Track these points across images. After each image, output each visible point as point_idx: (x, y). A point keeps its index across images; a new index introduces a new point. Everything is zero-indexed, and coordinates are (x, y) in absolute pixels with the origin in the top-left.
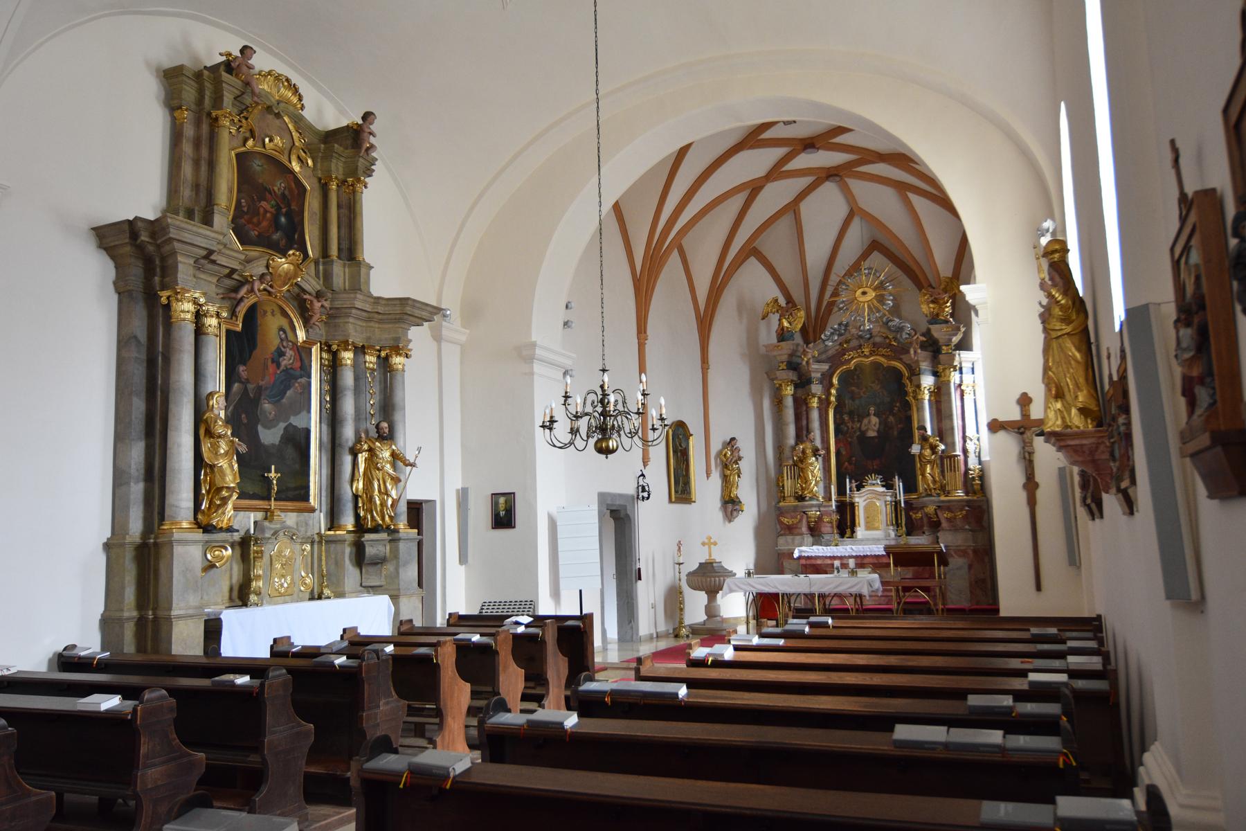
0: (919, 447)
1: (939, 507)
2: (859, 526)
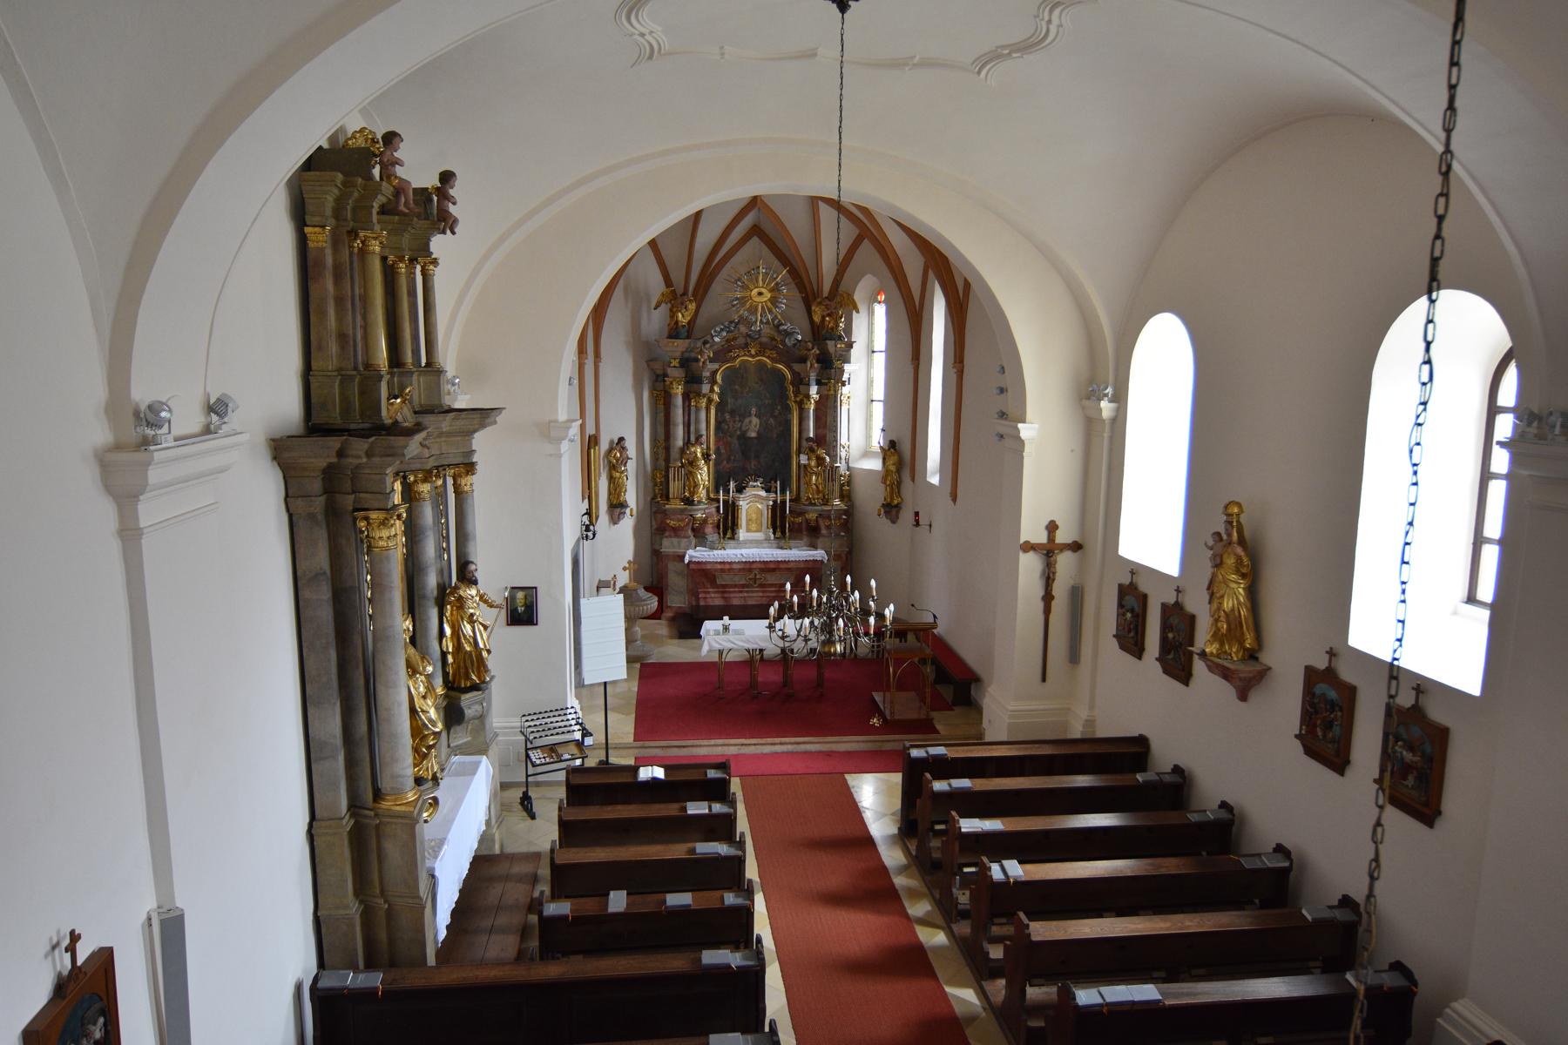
1: (820, 515)
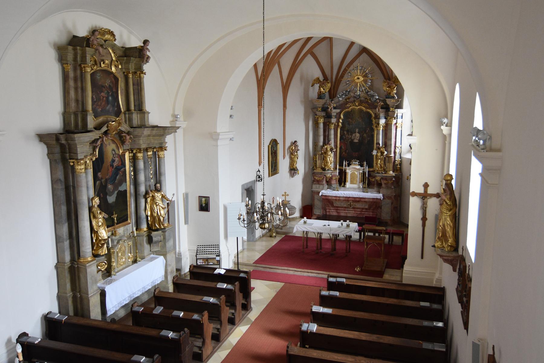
0: (376, 151)
1: (382, 178)
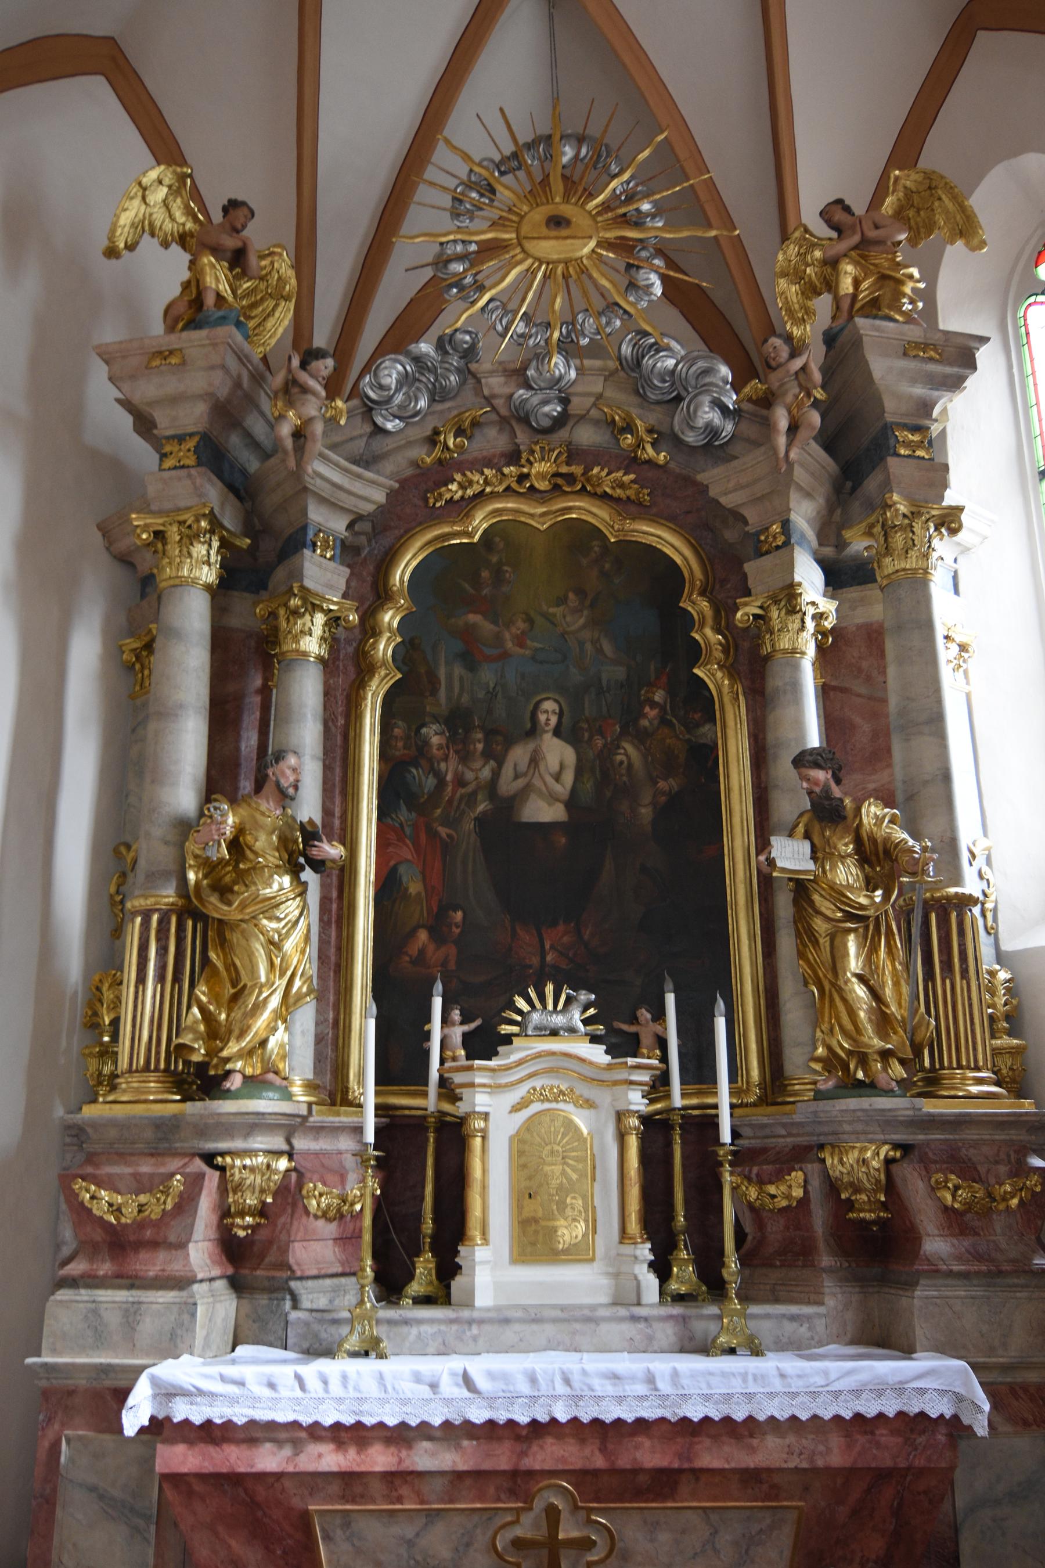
1: (906, 1148)
2: (486, 1241)
